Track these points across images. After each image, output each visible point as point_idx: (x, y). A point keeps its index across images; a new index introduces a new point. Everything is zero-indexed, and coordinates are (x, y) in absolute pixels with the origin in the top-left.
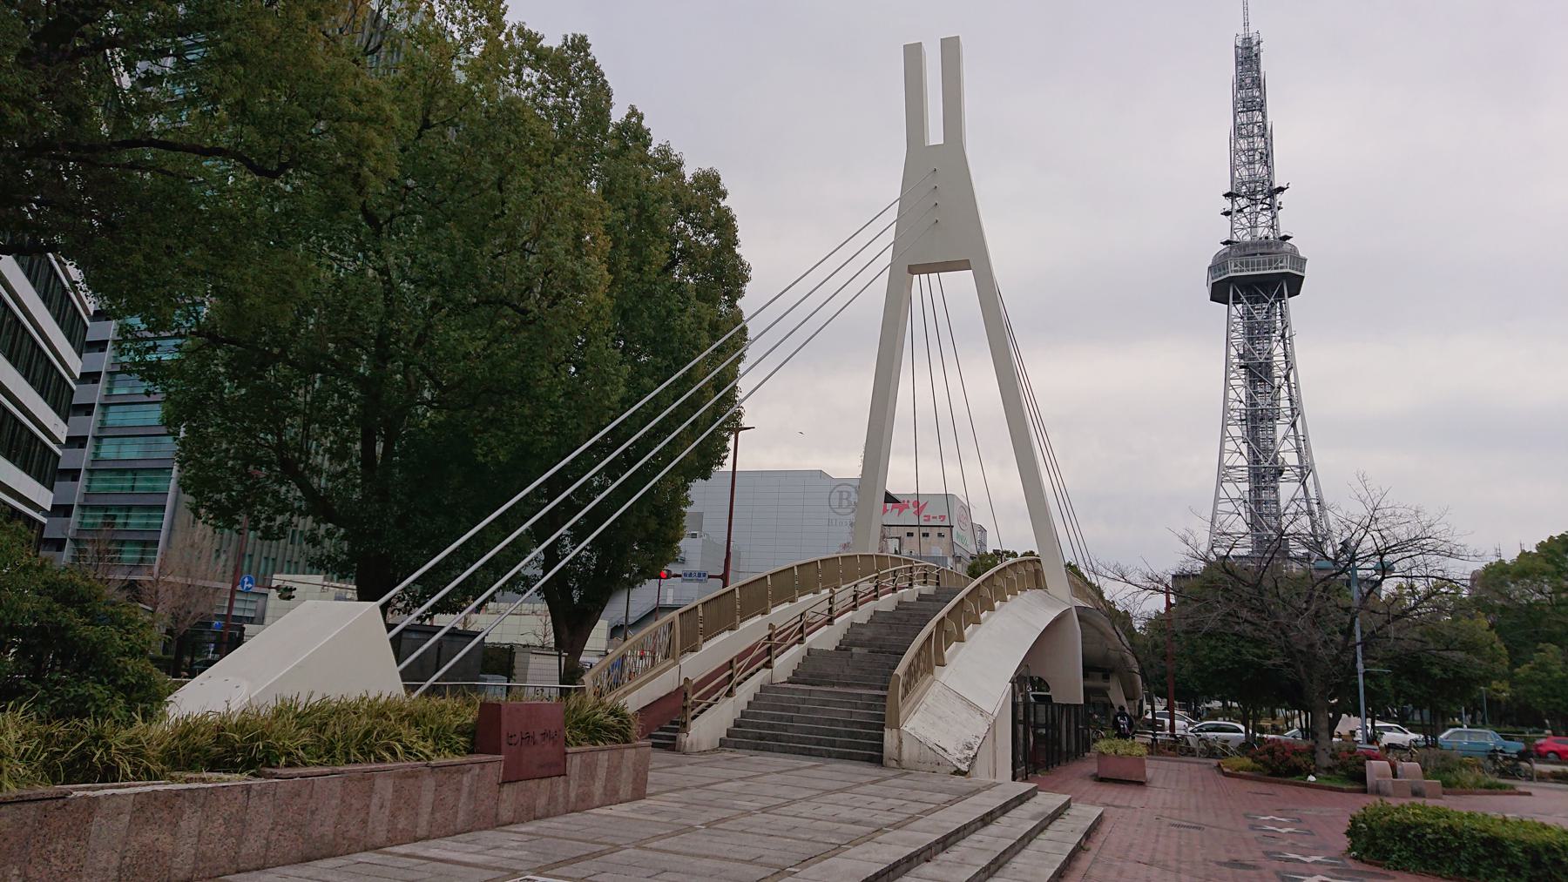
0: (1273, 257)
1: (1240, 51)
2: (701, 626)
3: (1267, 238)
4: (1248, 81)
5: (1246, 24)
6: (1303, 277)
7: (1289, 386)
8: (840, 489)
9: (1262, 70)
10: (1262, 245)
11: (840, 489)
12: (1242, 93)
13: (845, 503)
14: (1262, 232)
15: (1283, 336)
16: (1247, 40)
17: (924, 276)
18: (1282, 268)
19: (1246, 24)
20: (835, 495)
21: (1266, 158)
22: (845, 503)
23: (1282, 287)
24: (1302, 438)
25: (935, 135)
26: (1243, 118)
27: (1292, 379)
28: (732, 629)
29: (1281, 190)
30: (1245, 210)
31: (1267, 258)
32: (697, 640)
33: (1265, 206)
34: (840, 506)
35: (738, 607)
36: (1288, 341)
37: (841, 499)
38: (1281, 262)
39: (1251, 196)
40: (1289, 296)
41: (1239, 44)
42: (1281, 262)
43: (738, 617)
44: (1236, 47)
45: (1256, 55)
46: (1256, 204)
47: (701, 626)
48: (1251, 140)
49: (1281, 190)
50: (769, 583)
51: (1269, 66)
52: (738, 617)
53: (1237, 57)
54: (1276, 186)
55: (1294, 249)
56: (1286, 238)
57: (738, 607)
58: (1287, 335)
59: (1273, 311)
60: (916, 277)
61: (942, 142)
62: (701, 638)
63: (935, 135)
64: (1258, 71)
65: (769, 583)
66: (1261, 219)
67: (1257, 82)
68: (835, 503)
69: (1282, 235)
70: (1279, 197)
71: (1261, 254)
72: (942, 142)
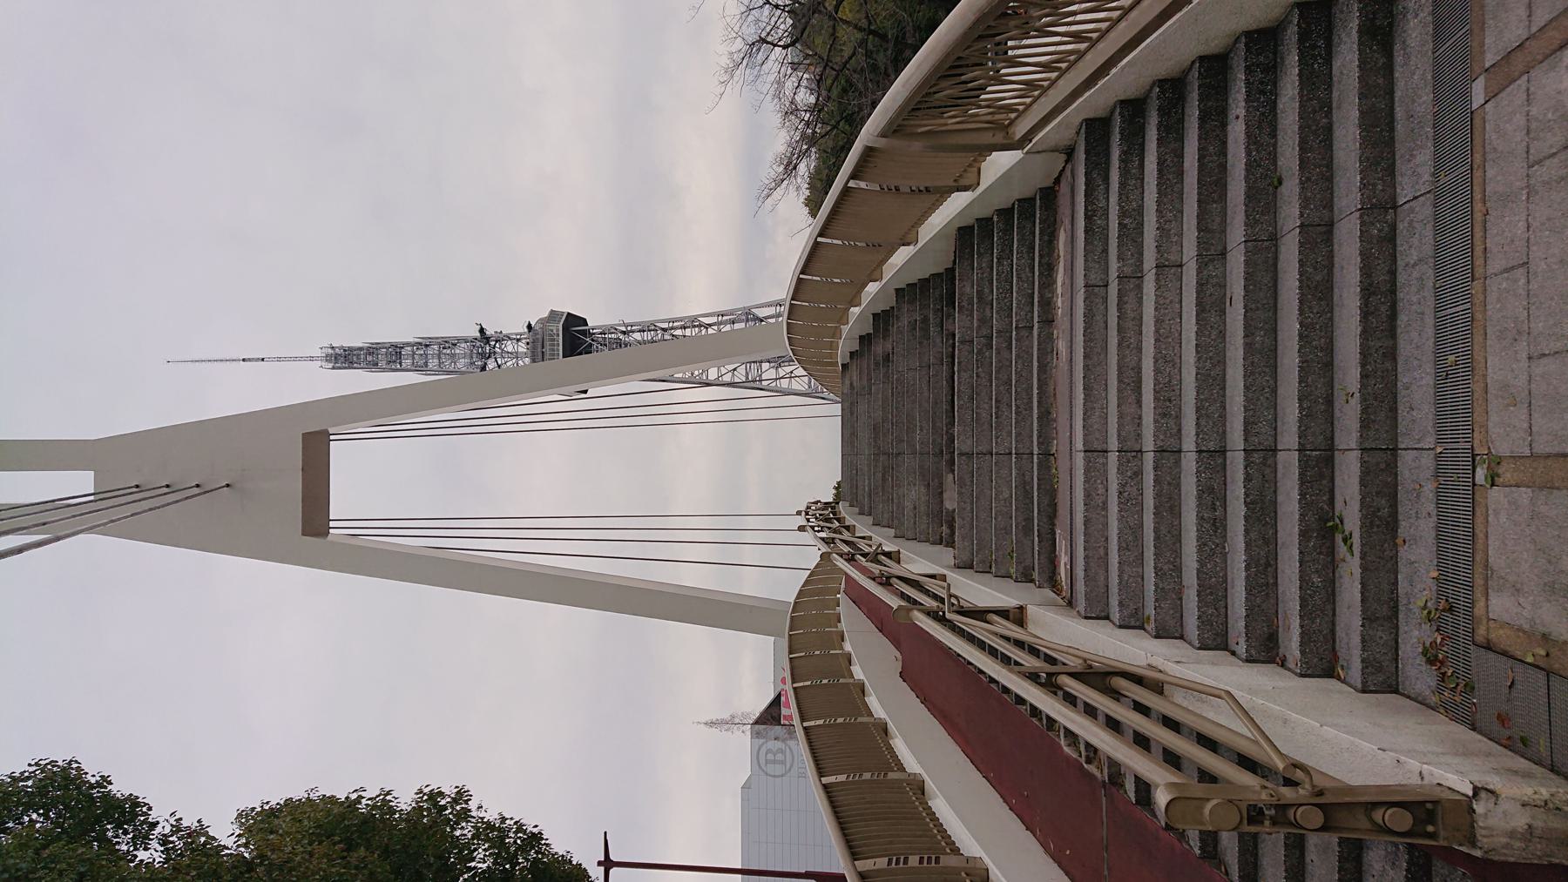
0: (547, 338)
1: (337, 365)
2: (914, 861)
3: (528, 344)
4: (370, 358)
5: (312, 359)
6: (569, 313)
7: (672, 328)
8: (762, 761)
9: (361, 345)
10: (534, 348)
11: (762, 761)
12: (382, 364)
13: (780, 757)
14: (522, 348)
15: (624, 333)
16: (328, 358)
17: (332, 524)
18: (558, 330)
19: (312, 359)
20: (770, 769)
21: (448, 343)
22: (780, 757)
23: (574, 331)
24: (720, 318)
25: (79, 483)
26: (407, 363)
27: (665, 325)
28: (920, 788)
29: (482, 331)
30: (499, 363)
31: (547, 343)
32: (956, 871)
33: (497, 345)
34: (783, 762)
35: (867, 776)
36: (629, 328)
37: (774, 762)
38: (552, 331)
39: (485, 356)
40: (587, 325)
41: (331, 365)
42: (552, 331)
43: (891, 775)
44: (333, 368)
45: (345, 350)
46: (495, 353)
47: (914, 861)
48: (430, 357)
49: (482, 331)
50: (842, 778)
51: (356, 339)
52: (891, 775)
53: (345, 368)
54: (479, 335)
55: (541, 321)
56: (529, 326)
57: (867, 776)
58: (624, 329)
59: (600, 340)
60: (331, 531)
61: (92, 473)
62: (948, 861)
63: (79, 483)
64: (361, 349)
65: (842, 778)
66: (510, 349)
67: (371, 350)
68: (779, 769)
69: (526, 330)
70: (490, 331)
71: (543, 347)
72: (92, 473)
